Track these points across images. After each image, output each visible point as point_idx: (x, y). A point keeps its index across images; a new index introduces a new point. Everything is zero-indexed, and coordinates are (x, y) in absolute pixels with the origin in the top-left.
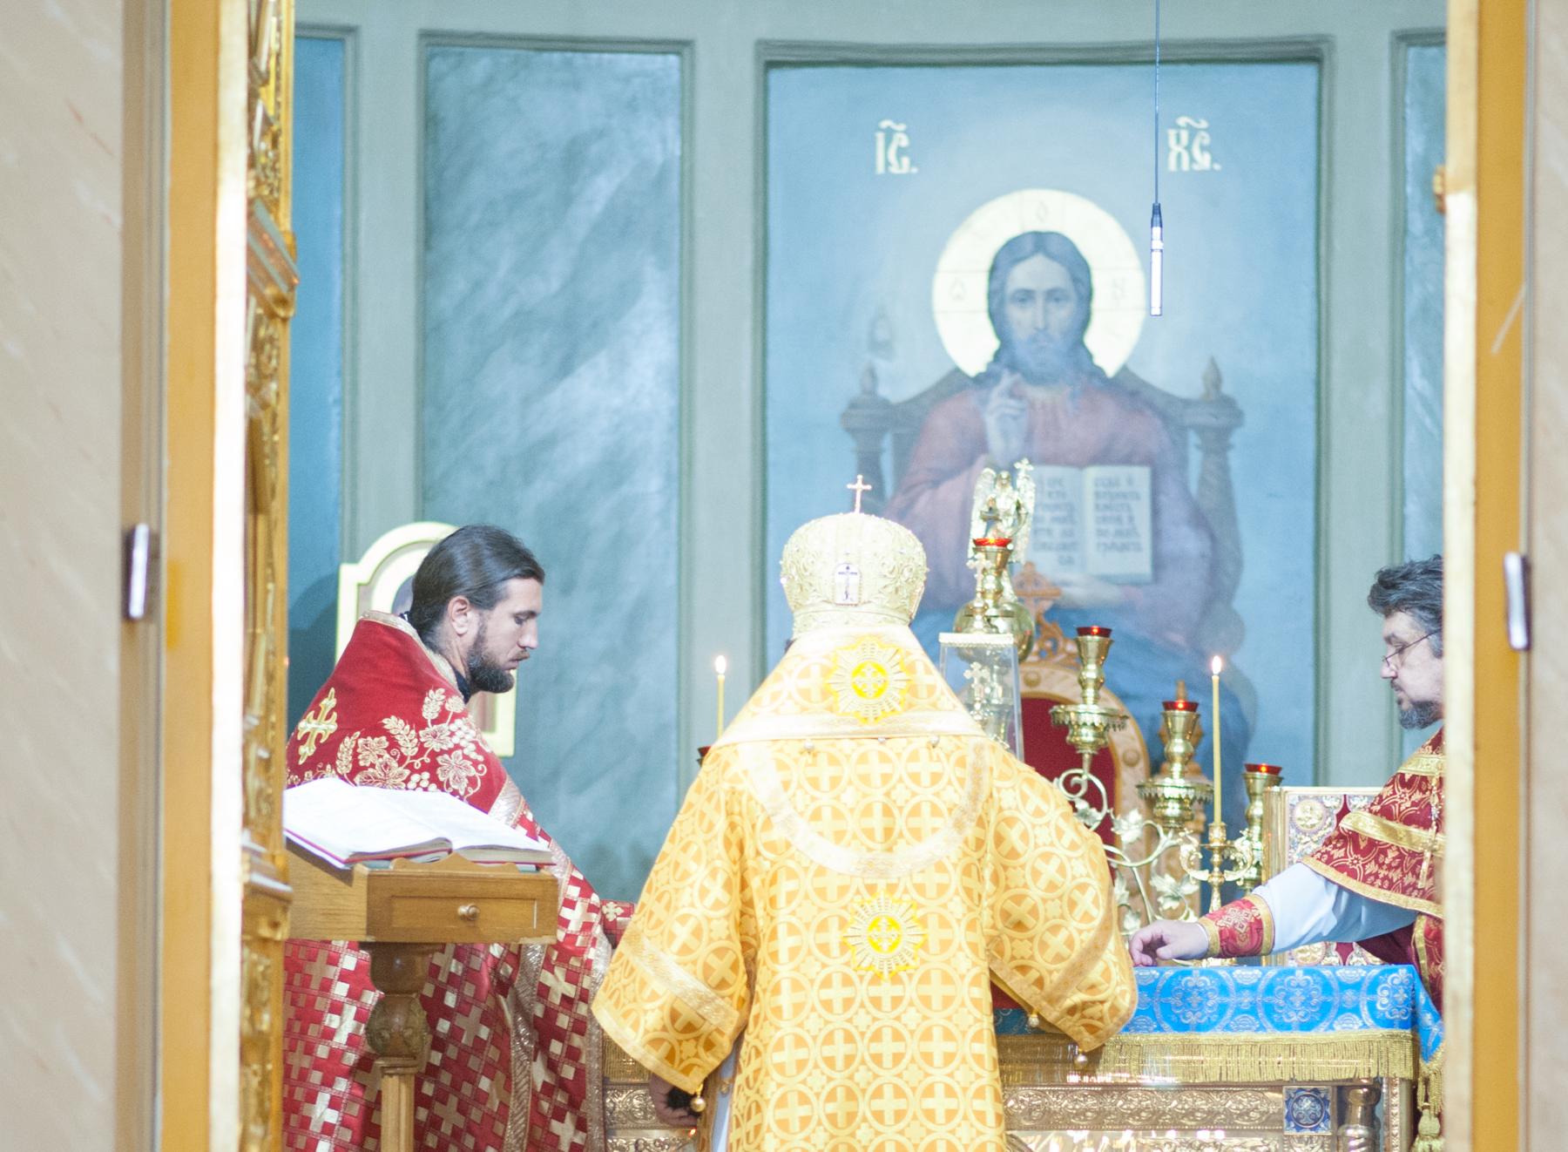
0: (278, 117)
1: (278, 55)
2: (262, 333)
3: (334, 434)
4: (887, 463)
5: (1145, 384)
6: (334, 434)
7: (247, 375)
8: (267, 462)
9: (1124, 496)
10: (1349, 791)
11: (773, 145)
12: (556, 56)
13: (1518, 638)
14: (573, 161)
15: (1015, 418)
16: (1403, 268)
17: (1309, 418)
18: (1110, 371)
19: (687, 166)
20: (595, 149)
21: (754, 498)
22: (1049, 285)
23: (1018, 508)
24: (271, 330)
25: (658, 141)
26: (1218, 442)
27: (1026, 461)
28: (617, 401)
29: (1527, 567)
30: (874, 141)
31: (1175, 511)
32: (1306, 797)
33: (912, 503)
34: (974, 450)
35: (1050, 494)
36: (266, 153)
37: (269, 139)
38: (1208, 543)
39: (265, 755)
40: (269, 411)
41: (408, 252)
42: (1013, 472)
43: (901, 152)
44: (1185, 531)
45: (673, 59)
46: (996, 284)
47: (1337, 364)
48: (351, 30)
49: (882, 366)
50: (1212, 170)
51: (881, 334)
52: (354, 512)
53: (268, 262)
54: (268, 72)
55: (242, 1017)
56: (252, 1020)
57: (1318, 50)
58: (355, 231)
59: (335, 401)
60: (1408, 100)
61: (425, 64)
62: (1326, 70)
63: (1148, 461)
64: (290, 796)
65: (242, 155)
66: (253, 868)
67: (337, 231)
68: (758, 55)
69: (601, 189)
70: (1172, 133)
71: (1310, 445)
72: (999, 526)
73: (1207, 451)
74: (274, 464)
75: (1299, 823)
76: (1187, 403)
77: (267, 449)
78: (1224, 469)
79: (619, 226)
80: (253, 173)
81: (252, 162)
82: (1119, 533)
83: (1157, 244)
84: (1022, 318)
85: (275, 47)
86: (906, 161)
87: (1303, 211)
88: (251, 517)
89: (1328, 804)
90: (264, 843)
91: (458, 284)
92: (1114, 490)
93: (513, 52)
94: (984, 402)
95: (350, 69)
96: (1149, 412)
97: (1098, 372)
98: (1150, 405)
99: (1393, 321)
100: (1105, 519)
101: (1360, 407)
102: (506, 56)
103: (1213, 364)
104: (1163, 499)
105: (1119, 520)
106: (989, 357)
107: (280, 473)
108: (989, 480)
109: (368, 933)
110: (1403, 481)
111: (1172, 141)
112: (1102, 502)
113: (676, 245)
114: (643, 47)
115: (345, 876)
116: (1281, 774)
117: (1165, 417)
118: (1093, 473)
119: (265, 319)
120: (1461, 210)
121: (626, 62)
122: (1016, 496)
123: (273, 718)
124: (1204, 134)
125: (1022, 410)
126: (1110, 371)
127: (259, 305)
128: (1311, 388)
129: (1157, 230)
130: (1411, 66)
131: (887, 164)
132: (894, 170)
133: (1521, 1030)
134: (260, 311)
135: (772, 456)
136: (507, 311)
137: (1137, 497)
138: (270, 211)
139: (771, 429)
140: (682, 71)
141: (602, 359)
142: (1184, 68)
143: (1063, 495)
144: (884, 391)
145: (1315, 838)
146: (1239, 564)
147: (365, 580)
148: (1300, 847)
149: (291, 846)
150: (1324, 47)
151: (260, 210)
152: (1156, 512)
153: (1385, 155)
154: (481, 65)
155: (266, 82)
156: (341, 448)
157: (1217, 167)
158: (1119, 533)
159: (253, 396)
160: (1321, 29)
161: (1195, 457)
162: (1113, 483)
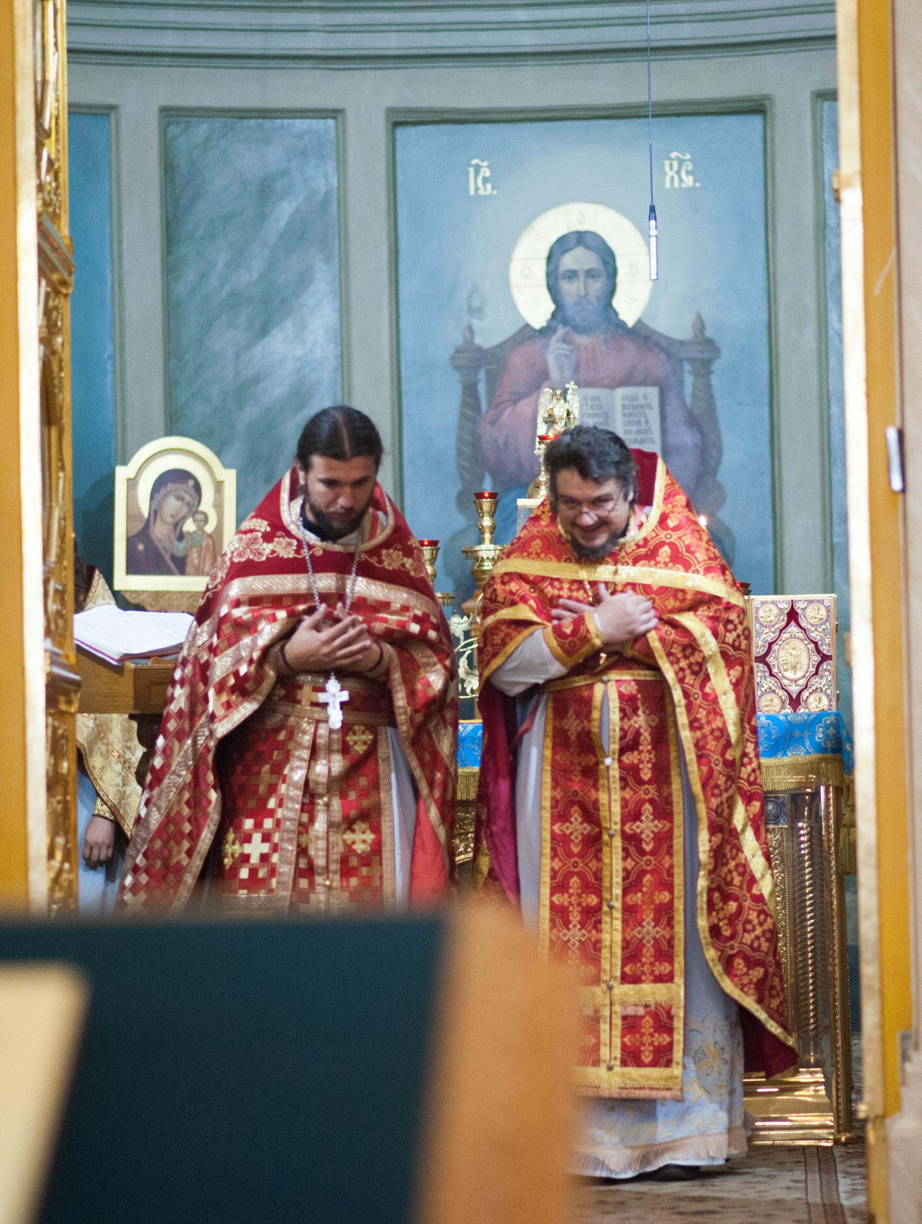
0: (58, 159)
1: (57, 118)
2: (51, 304)
3: (109, 379)
4: (482, 388)
5: (654, 332)
6: (109, 379)
7: (40, 332)
8: (56, 390)
9: (642, 407)
10: (795, 597)
11: (400, 178)
12: (252, 122)
13: (897, 484)
14: (266, 192)
15: (567, 356)
16: (824, 249)
17: (765, 355)
18: (630, 323)
19: (342, 193)
20: (279, 184)
21: (393, 416)
22: (587, 267)
23: (568, 414)
24: (57, 302)
25: (323, 178)
26: (704, 368)
27: (572, 383)
28: (299, 352)
29: (901, 435)
30: (468, 173)
31: (676, 416)
32: (766, 602)
33: (499, 416)
34: (540, 378)
35: (592, 407)
36: (50, 184)
37: (52, 173)
38: (699, 436)
39: (60, 588)
40: (57, 357)
41: (155, 257)
42: (565, 392)
43: (485, 181)
44: (683, 429)
45: (331, 122)
46: (552, 267)
47: (782, 314)
48: (113, 108)
49: (477, 324)
50: (694, 186)
51: (476, 303)
52: (124, 430)
53: (53, 256)
54: (50, 129)
55: (49, 764)
56: (56, 766)
57: (762, 105)
58: (120, 242)
59: (109, 357)
60: (824, 138)
61: (163, 130)
62: (769, 120)
63: (657, 383)
64: (77, 617)
65: (33, 183)
66: (53, 663)
67: (107, 242)
68: (388, 118)
69: (285, 210)
70: (667, 163)
71: (765, 368)
72: (556, 426)
73: (697, 376)
74: (61, 391)
75: (762, 620)
76: (682, 343)
77: (56, 382)
78: (709, 387)
79: (297, 235)
80: (40, 195)
81: (40, 188)
82: (639, 432)
83: (653, 232)
84: (570, 289)
85: (55, 113)
86: (489, 186)
87: (756, 212)
88: (46, 428)
89: (781, 606)
90: (61, 646)
91: (190, 276)
92: (635, 403)
93: (223, 120)
94: (546, 346)
95: (114, 135)
96: (657, 350)
97: (622, 325)
98: (658, 345)
99: (818, 285)
100: (629, 423)
101: (797, 342)
102: (218, 123)
103: (699, 317)
104: (668, 408)
105: (639, 423)
106: (549, 316)
107: (66, 398)
108: (548, 396)
109: (135, 709)
110: (828, 391)
111: (667, 169)
112: (627, 411)
113: (337, 246)
114: (310, 114)
115: (118, 670)
116: (749, 589)
117: (668, 355)
118: (620, 392)
119: (52, 295)
120: (852, 202)
121: (299, 125)
122: (567, 406)
123: (65, 563)
124: (688, 163)
125: (572, 351)
126: (630, 323)
127: (48, 285)
128: (765, 332)
129: (653, 223)
130: (825, 115)
131: (477, 188)
132: (481, 192)
133: (907, 746)
134: (49, 289)
135: (404, 386)
136: (224, 294)
137: (650, 407)
138: (54, 222)
139: (403, 368)
140: (337, 129)
141: (289, 324)
142: (674, 119)
143: (600, 407)
144: (479, 341)
145: (773, 630)
146: (720, 450)
147: (132, 476)
148: (763, 636)
149: (79, 649)
150: (767, 102)
151: (47, 223)
152: (663, 417)
153: (810, 174)
154: (202, 129)
155: (48, 135)
156: (114, 388)
157: (698, 185)
158: (639, 432)
159: (45, 346)
160: (766, 91)
161: (689, 379)
162: (634, 398)
